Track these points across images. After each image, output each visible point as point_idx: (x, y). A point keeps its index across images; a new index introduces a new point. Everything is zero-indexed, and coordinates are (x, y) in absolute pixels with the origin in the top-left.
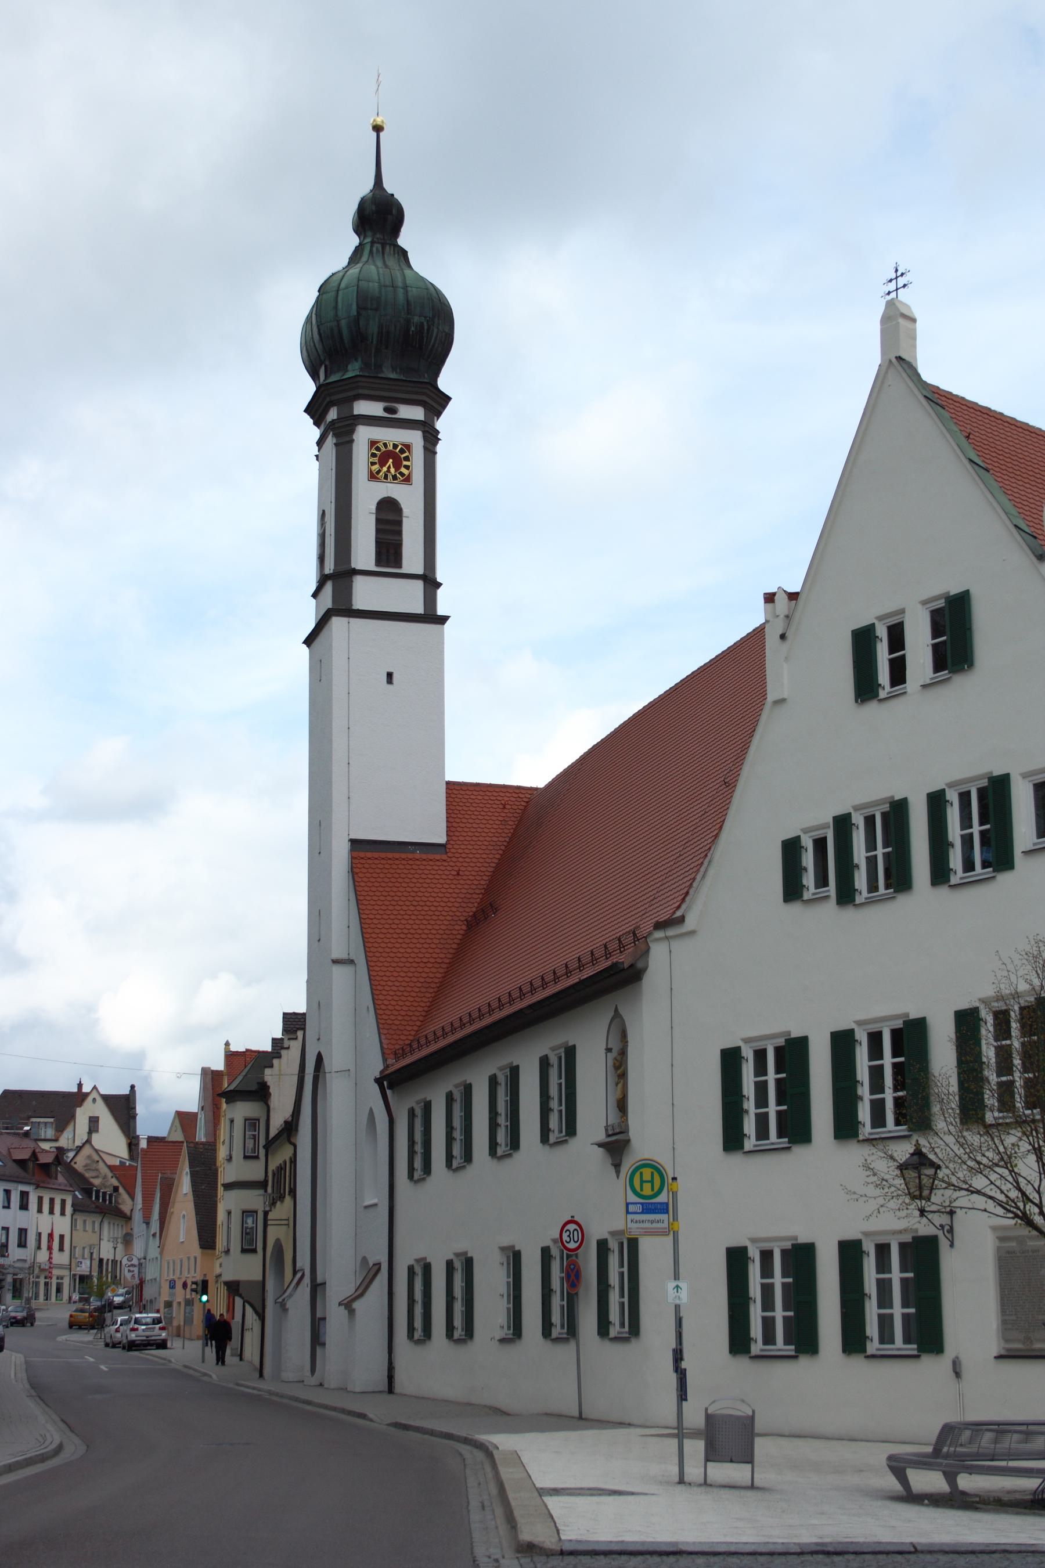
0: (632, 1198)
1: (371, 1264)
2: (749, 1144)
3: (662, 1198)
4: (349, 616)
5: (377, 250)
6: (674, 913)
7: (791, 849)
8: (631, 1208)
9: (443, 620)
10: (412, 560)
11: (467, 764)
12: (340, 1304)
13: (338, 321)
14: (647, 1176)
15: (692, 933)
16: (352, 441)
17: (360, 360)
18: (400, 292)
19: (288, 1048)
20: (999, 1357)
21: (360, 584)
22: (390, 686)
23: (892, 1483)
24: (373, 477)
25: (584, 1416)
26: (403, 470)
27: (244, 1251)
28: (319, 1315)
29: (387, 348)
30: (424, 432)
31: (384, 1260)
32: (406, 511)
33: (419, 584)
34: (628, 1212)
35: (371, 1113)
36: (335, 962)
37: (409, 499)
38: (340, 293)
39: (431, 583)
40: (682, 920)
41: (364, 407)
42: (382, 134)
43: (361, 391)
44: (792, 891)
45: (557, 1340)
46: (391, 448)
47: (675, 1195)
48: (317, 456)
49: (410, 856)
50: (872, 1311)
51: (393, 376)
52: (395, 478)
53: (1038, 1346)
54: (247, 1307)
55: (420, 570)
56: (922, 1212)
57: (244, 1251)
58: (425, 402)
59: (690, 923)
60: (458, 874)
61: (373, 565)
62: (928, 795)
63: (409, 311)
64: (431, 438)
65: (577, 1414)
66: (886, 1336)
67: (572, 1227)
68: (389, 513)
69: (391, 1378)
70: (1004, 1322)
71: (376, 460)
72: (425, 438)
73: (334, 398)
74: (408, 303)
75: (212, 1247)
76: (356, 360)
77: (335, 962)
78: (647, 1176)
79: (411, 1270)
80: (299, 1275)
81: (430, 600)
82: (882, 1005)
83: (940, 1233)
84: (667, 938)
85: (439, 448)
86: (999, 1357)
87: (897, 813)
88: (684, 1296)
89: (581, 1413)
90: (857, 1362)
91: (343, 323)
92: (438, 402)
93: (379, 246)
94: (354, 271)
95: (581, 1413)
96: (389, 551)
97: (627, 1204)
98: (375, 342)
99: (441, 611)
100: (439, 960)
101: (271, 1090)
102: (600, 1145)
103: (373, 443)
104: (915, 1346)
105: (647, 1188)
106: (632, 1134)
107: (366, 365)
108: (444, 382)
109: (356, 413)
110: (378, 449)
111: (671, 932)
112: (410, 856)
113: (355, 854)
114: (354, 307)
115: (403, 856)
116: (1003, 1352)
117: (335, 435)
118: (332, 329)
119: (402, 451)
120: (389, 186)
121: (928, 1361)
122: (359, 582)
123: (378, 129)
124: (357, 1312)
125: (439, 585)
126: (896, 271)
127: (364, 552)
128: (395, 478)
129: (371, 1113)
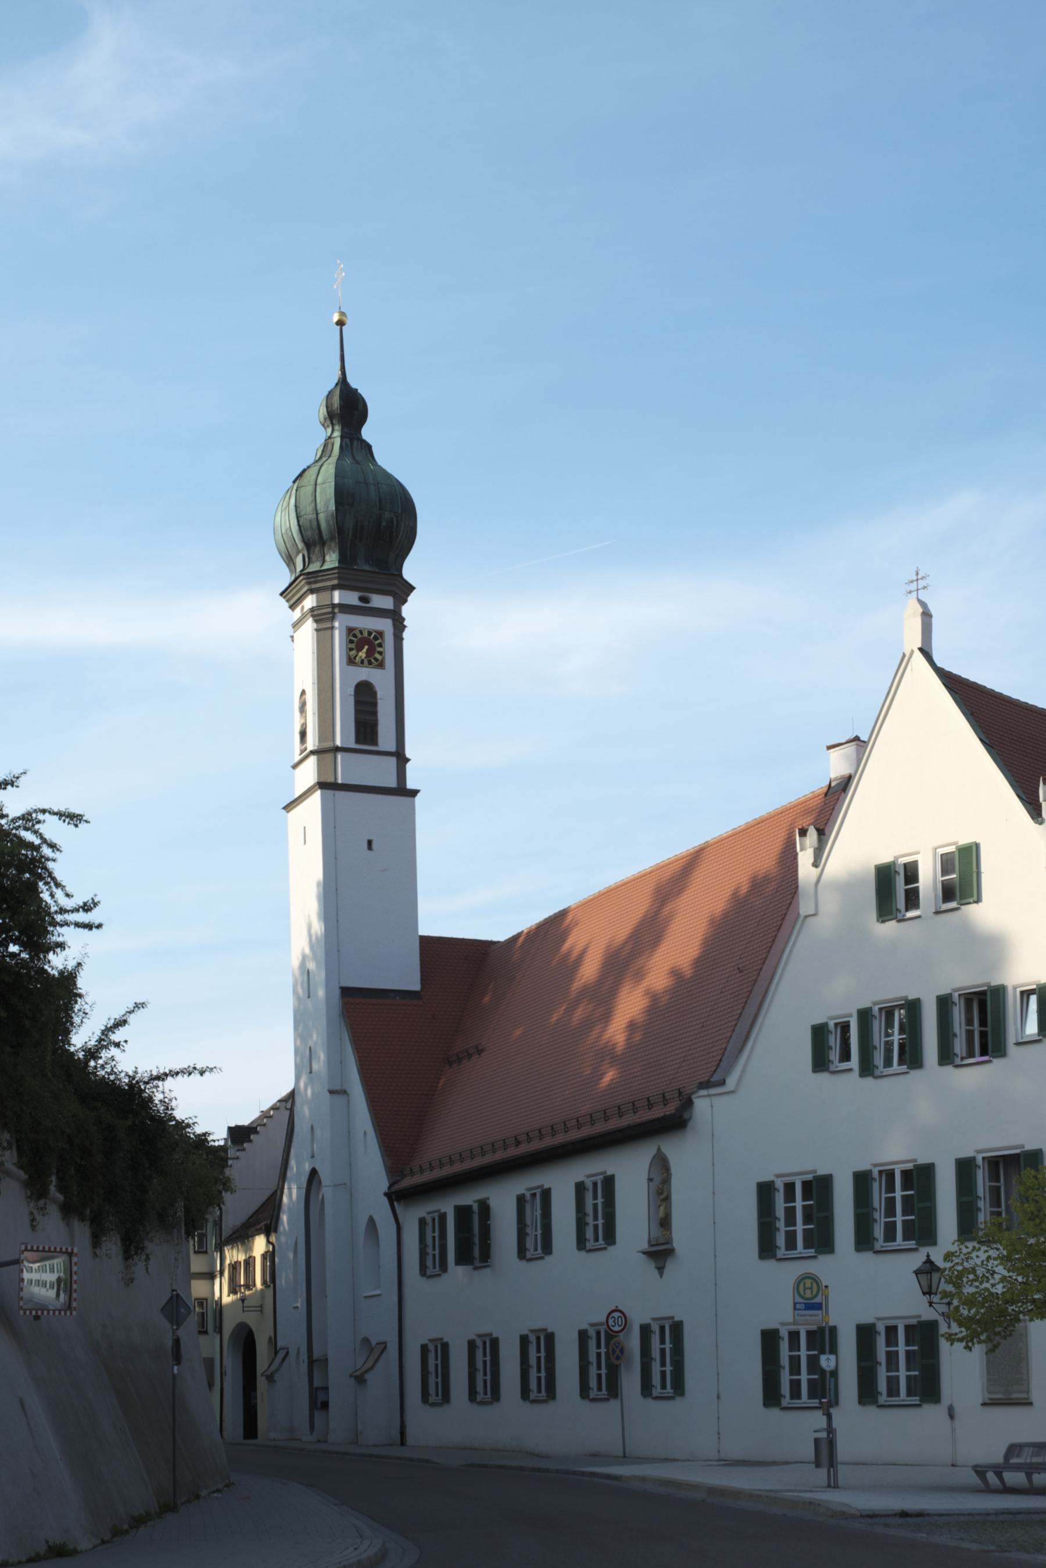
0: (798, 1299)
2: (781, 1252)
3: (818, 1300)
5: (347, 445)
6: (712, 1076)
7: (819, 1033)
8: (798, 1306)
9: (414, 793)
10: (386, 740)
12: (351, 1376)
13: (317, 514)
14: (808, 1285)
19: (237, 1158)
20: (984, 1404)
23: (976, 1480)
26: (377, 656)
28: (317, 1383)
33: (393, 760)
34: (795, 1309)
37: (381, 680)
39: (402, 760)
40: (723, 1083)
44: (820, 1063)
46: (366, 634)
47: (827, 1298)
51: (367, 568)
52: (370, 663)
53: (1015, 1396)
55: (392, 747)
56: (931, 1304)
59: (731, 1082)
62: (938, 997)
64: (399, 625)
65: (621, 1454)
67: (616, 1315)
70: (989, 1380)
71: (353, 646)
72: (394, 626)
74: (380, 500)
78: (808, 1285)
79: (424, 1349)
82: (897, 1151)
83: (941, 1319)
84: (709, 1095)
85: (405, 635)
86: (984, 1404)
87: (913, 1007)
88: (176, 1368)
89: (624, 1453)
90: (871, 1411)
91: (322, 517)
92: (403, 591)
93: (348, 440)
95: (624, 1453)
97: (795, 1304)
99: (410, 784)
102: (644, 1253)
103: (350, 630)
105: (808, 1292)
106: (675, 1245)
108: (410, 571)
110: (355, 636)
111: (713, 1091)
116: (988, 1401)
117: (316, 621)
118: (311, 521)
119: (376, 638)
120: (353, 382)
121: (929, 1409)
125: (408, 760)
126: (917, 574)
128: (370, 663)
129: (371, 1221)
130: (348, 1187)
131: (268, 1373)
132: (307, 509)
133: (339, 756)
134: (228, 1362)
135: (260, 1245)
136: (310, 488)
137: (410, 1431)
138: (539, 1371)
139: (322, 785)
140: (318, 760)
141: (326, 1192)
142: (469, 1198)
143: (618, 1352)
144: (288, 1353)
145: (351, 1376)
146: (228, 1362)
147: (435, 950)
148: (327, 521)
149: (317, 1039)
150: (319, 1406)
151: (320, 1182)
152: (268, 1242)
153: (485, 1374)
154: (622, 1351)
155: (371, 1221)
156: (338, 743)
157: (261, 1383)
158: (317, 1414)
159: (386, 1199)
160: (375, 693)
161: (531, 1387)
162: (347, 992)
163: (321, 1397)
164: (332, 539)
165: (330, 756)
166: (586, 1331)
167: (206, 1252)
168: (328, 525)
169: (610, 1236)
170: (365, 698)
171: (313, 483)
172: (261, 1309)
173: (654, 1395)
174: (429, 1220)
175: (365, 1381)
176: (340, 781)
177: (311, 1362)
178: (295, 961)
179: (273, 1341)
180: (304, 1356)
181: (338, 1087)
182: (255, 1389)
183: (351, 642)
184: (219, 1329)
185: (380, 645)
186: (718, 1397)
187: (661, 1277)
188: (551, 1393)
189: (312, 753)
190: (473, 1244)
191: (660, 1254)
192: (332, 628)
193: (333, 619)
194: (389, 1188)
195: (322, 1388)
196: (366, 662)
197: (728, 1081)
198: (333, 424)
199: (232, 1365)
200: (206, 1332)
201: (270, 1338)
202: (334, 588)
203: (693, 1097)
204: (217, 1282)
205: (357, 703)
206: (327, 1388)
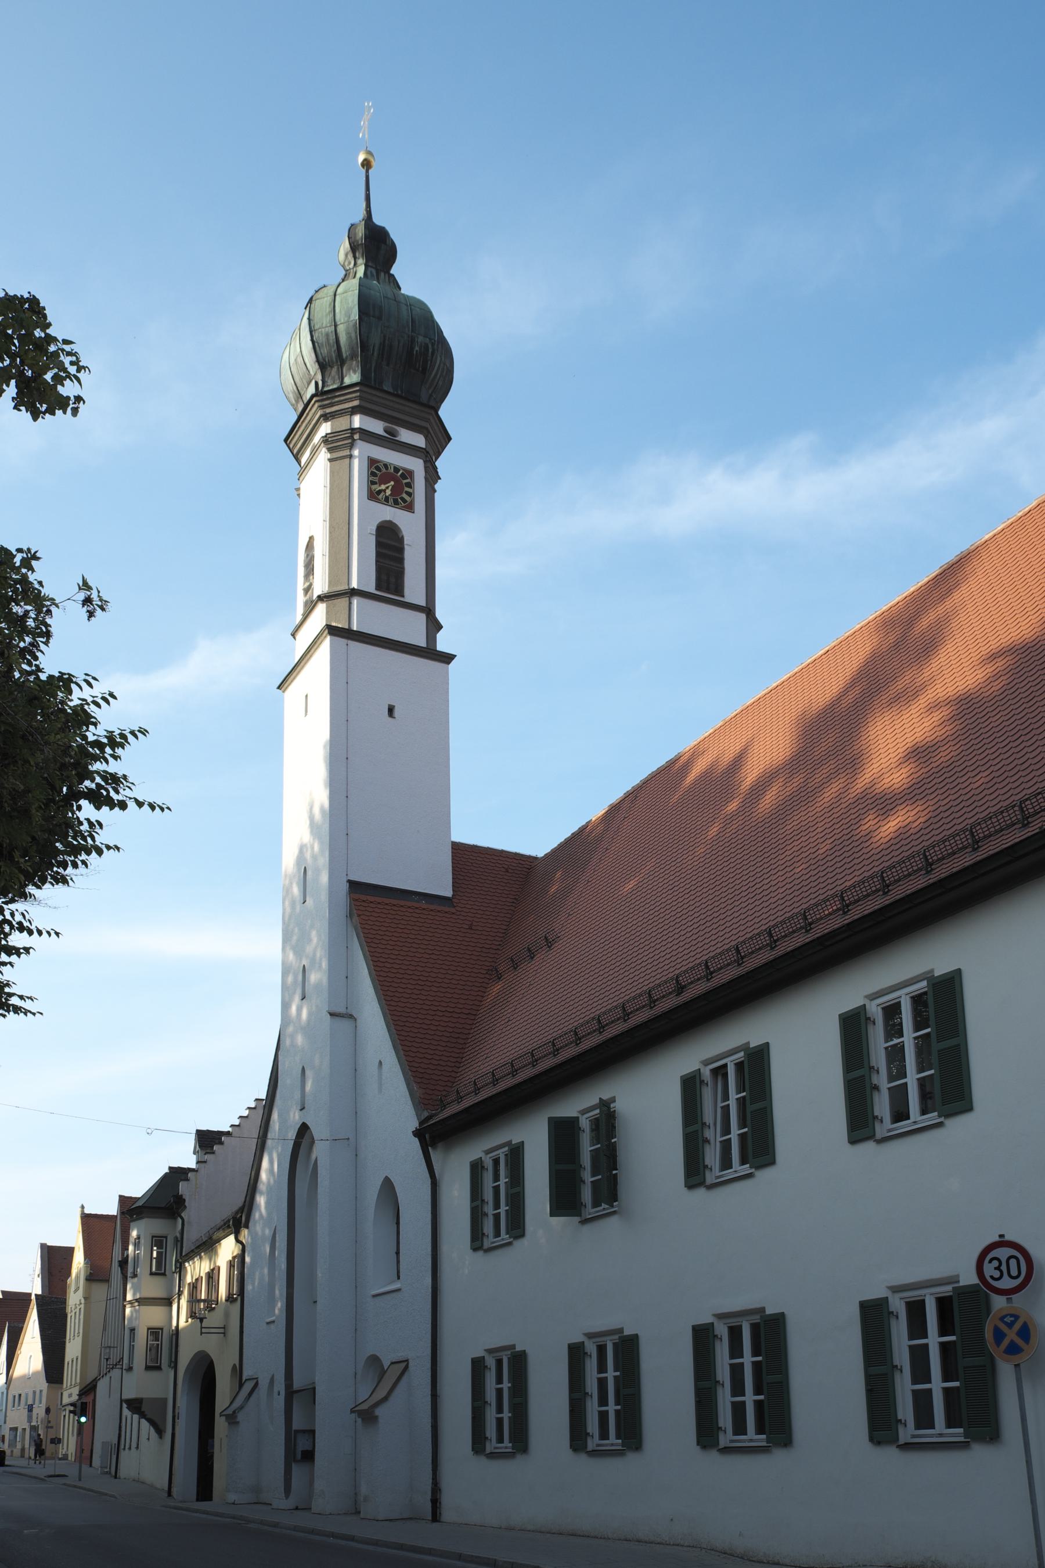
11: (467, 830)
12: (352, 1411)
13: (336, 326)
18: (404, 308)
22: (390, 719)
26: (404, 496)
27: (148, 1368)
29: (388, 365)
30: (425, 462)
31: (419, 1354)
33: (422, 617)
39: (434, 626)
45: (492, 1456)
52: (396, 502)
54: (143, 1421)
57: (148, 1368)
58: (427, 429)
64: (432, 476)
66: (924, 1419)
67: (1003, 1253)
69: (435, 1502)
71: (376, 479)
75: (60, 1381)
79: (478, 1366)
80: (248, 1387)
81: (431, 638)
91: (341, 329)
93: (374, 271)
98: (376, 354)
101: (187, 1204)
103: (372, 462)
108: (447, 412)
115: (409, 904)
118: (327, 335)
119: (403, 476)
120: (378, 220)
129: (388, 1185)
130: (351, 1143)
131: (230, 1412)
132: (323, 321)
133: (355, 601)
134: (182, 1402)
135: (228, 1248)
136: (330, 299)
137: (447, 1499)
138: (500, 1410)
139: (332, 630)
140: (327, 608)
141: (320, 1151)
142: (577, 1105)
143: (1011, 1335)
144: (257, 1384)
145: (352, 1411)
146: (182, 1402)
147: (466, 857)
148: (348, 333)
149: (317, 942)
150: (299, 1456)
152: (238, 1241)
153: (500, 1410)
154: (1025, 1333)
155: (388, 1185)
156: (354, 584)
157: (220, 1425)
158: (296, 1469)
159: (416, 1141)
160: (401, 540)
162: (354, 886)
163: (302, 1444)
164: (353, 356)
165: (343, 602)
167: (164, 1274)
168: (349, 338)
170: (388, 545)
171: (332, 294)
172: (224, 1330)
174: (488, 1163)
175: (376, 1418)
176: (355, 629)
177: (290, 1394)
178: (289, 860)
179: (238, 1371)
180: (280, 1386)
181: (341, 1010)
182: (212, 1436)
183: (373, 474)
184: (174, 1364)
185: (409, 485)
189: (321, 598)
190: (589, 1179)
192: (351, 456)
193: (351, 446)
194: (421, 1124)
195: (304, 1432)
196: (391, 501)
198: (355, 258)
199: (187, 1407)
200: (159, 1368)
202: (353, 411)
204: (175, 1307)
205: (379, 544)
206: (312, 1432)
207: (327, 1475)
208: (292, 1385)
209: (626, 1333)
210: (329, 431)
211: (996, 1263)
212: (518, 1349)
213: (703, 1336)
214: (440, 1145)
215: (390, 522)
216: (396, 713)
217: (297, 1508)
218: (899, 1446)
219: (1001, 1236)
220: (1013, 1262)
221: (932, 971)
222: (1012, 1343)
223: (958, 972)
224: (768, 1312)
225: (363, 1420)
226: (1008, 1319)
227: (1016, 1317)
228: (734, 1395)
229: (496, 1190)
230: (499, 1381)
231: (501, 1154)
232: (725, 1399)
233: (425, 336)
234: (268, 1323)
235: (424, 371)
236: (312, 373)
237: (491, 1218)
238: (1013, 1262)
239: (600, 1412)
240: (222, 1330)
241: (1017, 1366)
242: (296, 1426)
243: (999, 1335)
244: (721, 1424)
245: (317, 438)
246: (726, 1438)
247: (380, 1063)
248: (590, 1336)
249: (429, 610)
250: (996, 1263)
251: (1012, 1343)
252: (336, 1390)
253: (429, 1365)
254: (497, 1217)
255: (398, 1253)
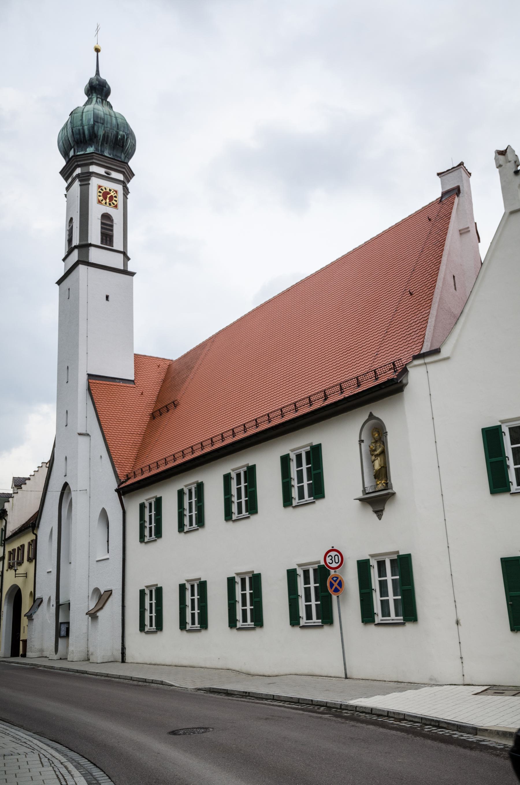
1: (102, 592)
4: (88, 266)
9: (132, 274)
10: (118, 244)
11: (144, 346)
12: (87, 614)
13: (83, 127)
15: (447, 359)
16: (89, 184)
17: (93, 147)
18: (114, 119)
19: (17, 493)
21: (93, 251)
22: (107, 302)
24: (99, 202)
25: (348, 676)
26: (114, 202)
30: (123, 186)
32: (115, 221)
33: (122, 256)
35: (104, 513)
36: (80, 434)
37: (117, 215)
38: (84, 114)
39: (127, 258)
41: (93, 169)
42: (99, 53)
43: (94, 161)
45: (148, 633)
48: (66, 195)
49: (118, 384)
50: (377, 598)
58: (124, 172)
59: (445, 352)
60: (142, 394)
61: (93, 246)
63: (118, 129)
64: (126, 191)
65: (344, 676)
66: (386, 612)
67: (333, 554)
68: (106, 217)
69: (123, 654)
73: (79, 163)
76: (92, 147)
77: (80, 434)
79: (142, 593)
89: (346, 674)
91: (86, 128)
92: (129, 175)
93: (100, 100)
94: (90, 107)
95: (346, 674)
96: (107, 237)
99: (130, 269)
100: (139, 433)
101: (8, 513)
102: (361, 500)
104: (402, 618)
107: (97, 149)
108: (132, 163)
109: (91, 171)
110: (102, 190)
112: (118, 384)
113: (90, 381)
114: (92, 120)
115: (115, 384)
117: (80, 181)
118: (79, 130)
122: (92, 250)
123: (97, 50)
124: (99, 618)
127: (95, 236)
128: (110, 204)
129: (104, 513)
131: (29, 614)
137: (128, 652)
138: (151, 612)
143: (336, 585)
145: (87, 614)
151: (70, 489)
153: (151, 612)
154: (340, 584)
157: (24, 621)
158: (60, 641)
159: (116, 494)
161: (146, 623)
166: (295, 570)
169: (318, 491)
173: (301, 624)
175: (98, 616)
177: (58, 606)
179: (33, 594)
180: (53, 602)
186: (458, 623)
187: (380, 519)
188: (204, 624)
189: (76, 247)
191: (378, 499)
194: (119, 486)
196: (108, 204)
197: (442, 351)
201: (31, 592)
203: (407, 367)
206: (68, 623)
207: (75, 646)
208: (59, 601)
209: (202, 580)
210: (80, 172)
211: (330, 558)
212: (159, 586)
213: (231, 582)
214: (127, 495)
215: (107, 213)
216: (110, 298)
217: (61, 659)
218: (300, 627)
219: (333, 547)
220: (336, 557)
221: (312, 443)
222: (336, 588)
223: (320, 445)
224: (255, 573)
225: (92, 618)
226: (335, 579)
227: (337, 578)
228: (306, 601)
229: (150, 516)
230: (151, 599)
231: (153, 501)
232: (302, 603)
233: (123, 132)
234: (48, 572)
235: (123, 146)
236: (72, 145)
237: (148, 529)
238: (336, 557)
239: (243, 610)
240: (25, 575)
241: (338, 597)
242: (60, 621)
243: (332, 585)
244: (301, 615)
245: (75, 174)
246: (239, 624)
247: (101, 457)
248: (188, 581)
249: (124, 253)
250: (330, 558)
251: (336, 588)
252: (80, 603)
253: (121, 592)
254: (150, 528)
255: (108, 541)
